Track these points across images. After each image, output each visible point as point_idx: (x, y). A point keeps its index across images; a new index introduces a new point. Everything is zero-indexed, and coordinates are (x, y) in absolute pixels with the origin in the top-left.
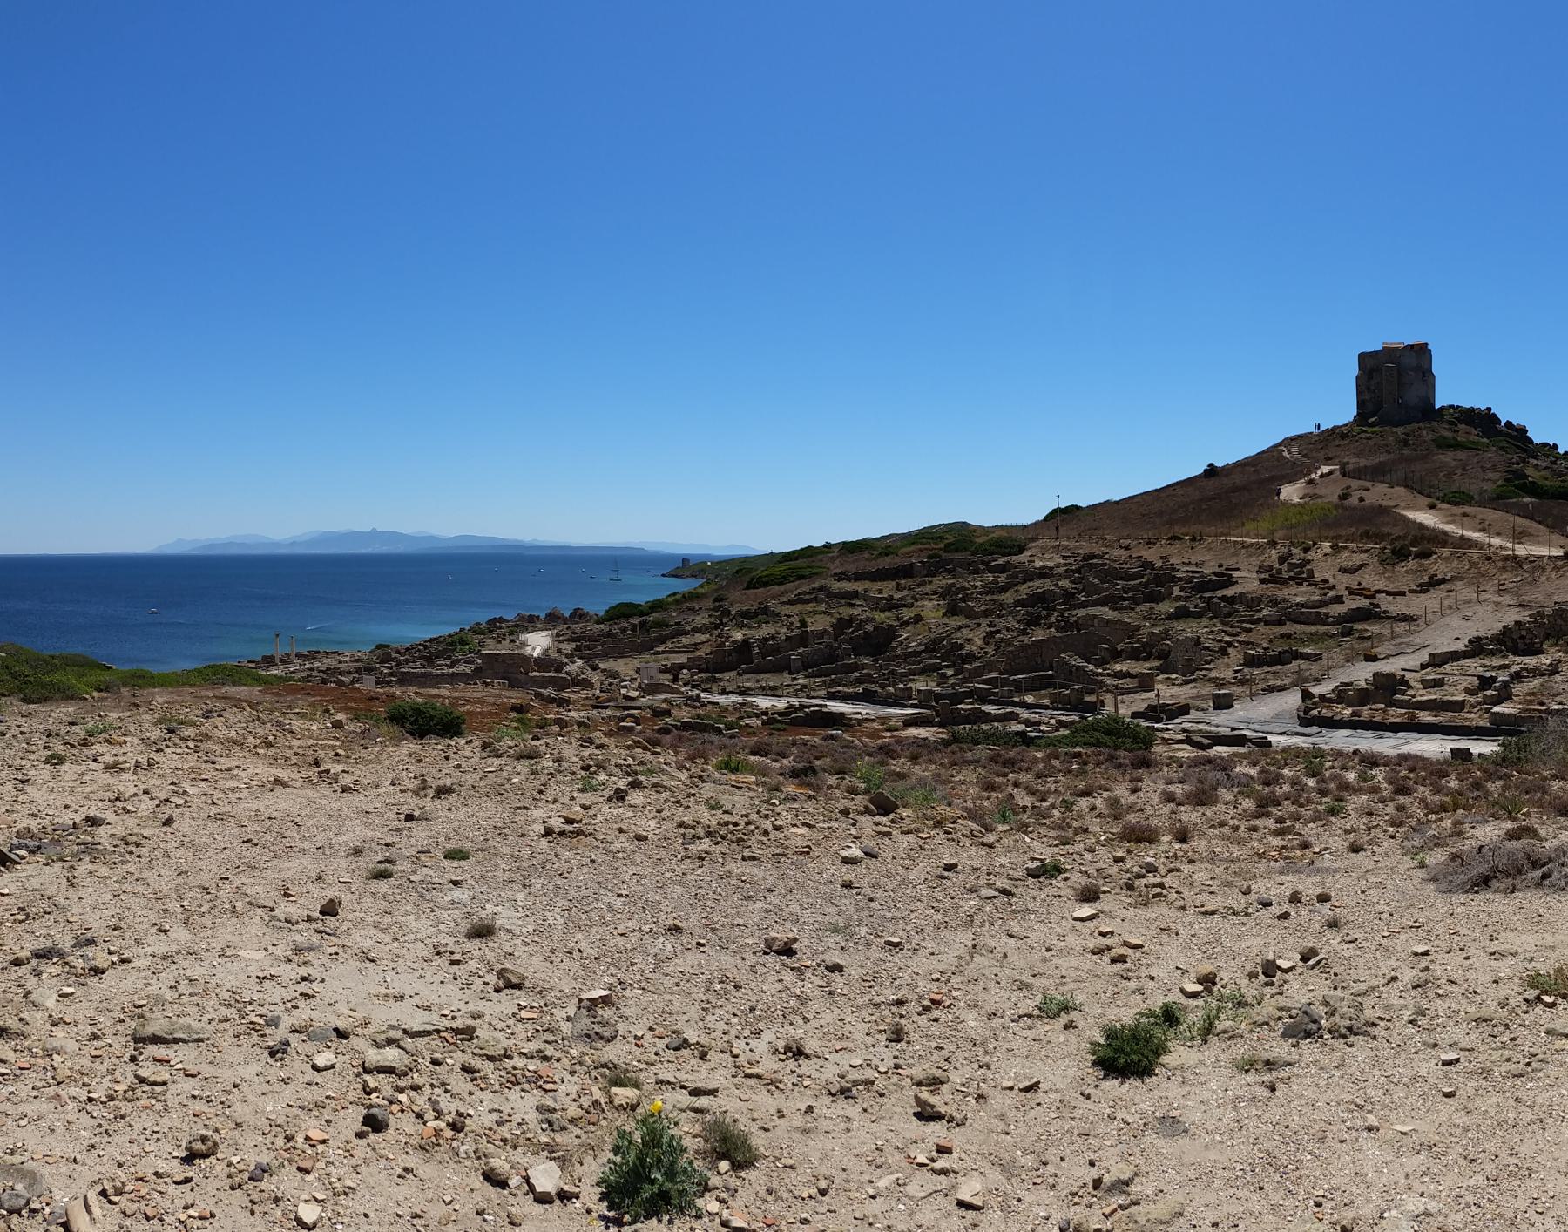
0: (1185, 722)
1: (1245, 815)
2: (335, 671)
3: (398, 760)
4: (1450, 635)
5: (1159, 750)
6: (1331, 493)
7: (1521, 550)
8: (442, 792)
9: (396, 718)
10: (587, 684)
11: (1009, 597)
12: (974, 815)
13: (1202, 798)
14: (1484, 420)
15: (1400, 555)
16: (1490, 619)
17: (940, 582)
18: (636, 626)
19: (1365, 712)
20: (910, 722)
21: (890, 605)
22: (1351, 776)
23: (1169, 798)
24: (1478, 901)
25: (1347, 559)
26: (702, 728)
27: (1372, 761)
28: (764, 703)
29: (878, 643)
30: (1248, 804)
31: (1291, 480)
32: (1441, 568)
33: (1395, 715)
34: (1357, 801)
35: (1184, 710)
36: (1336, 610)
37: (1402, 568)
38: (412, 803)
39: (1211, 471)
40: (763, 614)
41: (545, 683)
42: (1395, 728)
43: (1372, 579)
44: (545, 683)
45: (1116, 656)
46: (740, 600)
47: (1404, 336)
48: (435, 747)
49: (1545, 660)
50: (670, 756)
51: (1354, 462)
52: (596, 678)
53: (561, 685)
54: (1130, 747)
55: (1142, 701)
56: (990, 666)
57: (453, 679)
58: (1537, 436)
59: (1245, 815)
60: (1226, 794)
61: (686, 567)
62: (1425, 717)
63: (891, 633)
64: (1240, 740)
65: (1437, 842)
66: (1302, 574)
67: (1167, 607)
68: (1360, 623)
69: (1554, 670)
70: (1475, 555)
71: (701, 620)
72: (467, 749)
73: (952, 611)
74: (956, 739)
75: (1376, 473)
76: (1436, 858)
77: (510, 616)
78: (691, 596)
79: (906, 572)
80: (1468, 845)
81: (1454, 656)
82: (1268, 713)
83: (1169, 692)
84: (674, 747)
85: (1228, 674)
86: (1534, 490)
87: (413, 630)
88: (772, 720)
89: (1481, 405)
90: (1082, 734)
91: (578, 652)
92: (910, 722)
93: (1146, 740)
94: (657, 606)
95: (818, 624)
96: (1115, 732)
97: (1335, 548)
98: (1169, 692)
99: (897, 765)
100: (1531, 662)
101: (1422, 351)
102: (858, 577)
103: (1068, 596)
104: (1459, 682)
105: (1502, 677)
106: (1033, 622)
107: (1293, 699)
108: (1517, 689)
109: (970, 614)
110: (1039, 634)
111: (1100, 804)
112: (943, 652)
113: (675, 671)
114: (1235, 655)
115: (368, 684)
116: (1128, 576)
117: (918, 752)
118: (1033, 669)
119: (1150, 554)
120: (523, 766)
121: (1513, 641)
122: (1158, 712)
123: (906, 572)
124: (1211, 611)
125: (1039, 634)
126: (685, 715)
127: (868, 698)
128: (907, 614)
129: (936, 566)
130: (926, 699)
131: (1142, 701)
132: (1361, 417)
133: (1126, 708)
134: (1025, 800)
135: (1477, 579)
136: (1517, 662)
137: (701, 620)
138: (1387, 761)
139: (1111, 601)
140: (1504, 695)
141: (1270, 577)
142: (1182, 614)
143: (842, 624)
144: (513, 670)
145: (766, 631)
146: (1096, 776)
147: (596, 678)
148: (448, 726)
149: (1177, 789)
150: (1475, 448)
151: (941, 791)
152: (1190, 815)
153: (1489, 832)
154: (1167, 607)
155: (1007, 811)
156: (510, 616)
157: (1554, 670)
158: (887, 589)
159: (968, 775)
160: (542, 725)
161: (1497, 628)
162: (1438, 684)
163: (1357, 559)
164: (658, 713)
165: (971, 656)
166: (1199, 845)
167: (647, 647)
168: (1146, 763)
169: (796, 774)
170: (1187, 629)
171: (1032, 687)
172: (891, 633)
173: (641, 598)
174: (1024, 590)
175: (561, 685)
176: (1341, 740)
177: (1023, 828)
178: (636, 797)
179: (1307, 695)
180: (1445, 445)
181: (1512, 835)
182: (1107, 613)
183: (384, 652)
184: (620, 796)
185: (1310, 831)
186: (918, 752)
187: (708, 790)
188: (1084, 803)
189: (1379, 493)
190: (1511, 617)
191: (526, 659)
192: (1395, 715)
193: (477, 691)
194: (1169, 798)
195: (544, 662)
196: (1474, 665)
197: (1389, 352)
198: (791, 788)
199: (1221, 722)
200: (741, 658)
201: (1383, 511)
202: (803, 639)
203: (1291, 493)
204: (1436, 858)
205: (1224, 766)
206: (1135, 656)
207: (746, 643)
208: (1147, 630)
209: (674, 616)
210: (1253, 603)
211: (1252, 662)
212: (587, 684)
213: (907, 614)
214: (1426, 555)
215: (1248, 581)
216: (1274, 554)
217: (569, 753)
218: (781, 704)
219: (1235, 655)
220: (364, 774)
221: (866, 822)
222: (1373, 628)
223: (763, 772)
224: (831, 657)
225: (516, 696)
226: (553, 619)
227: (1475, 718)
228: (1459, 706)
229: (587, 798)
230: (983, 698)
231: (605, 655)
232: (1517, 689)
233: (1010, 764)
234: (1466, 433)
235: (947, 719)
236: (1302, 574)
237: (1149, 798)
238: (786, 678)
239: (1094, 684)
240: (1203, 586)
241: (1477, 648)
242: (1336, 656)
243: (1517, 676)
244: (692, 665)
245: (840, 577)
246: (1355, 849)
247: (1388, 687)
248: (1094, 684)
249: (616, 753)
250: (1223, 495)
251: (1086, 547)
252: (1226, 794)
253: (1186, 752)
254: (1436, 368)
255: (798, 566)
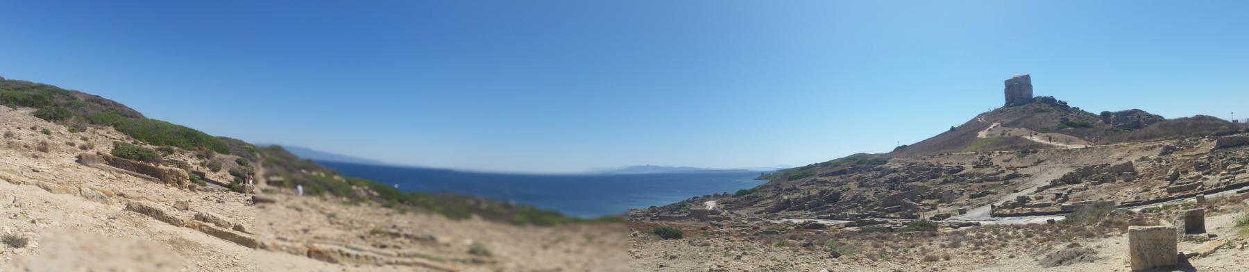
0: (949, 220)
1: (971, 249)
2: (636, 216)
3: (660, 246)
4: (1045, 180)
5: (940, 230)
6: (998, 133)
7: (1070, 147)
8: (672, 258)
9: (657, 233)
10: (729, 219)
11: (882, 180)
12: (869, 256)
13: (955, 245)
14: (1050, 101)
15: (1025, 153)
16: (1058, 173)
17: (856, 175)
18: (747, 198)
19: (1015, 211)
20: (847, 225)
21: (839, 185)
22: (1010, 233)
23: (943, 246)
24: (1059, 268)
25: (1005, 157)
26: (771, 233)
27: (1018, 227)
28: (795, 221)
29: (835, 198)
30: (972, 246)
31: (982, 129)
32: (1041, 156)
33: (1026, 210)
34: (1011, 242)
35: (949, 216)
36: (1002, 175)
37: (1027, 157)
38: (663, 261)
39: (953, 129)
40: (794, 190)
41: (713, 219)
42: (1026, 215)
43: (1015, 163)
44: (713, 219)
45: (923, 198)
46: (786, 185)
47: (1020, 73)
48: (671, 242)
49: (1083, 185)
50: (757, 243)
51: (1006, 121)
52: (732, 216)
53: (719, 220)
54: (929, 230)
55: (933, 213)
56: (877, 204)
57: (680, 218)
58: (1071, 105)
59: (971, 249)
60: (964, 243)
61: (763, 176)
62: (1037, 210)
63: (839, 195)
64: (970, 224)
65: (1042, 252)
66: (988, 164)
67: (940, 180)
68: (1011, 179)
69: (1086, 188)
70: (1053, 150)
71: (769, 195)
72: (683, 243)
73: (861, 185)
74: (863, 230)
75: (1014, 124)
76: (1042, 257)
77: (701, 196)
78: (765, 186)
79: (844, 172)
80: (1053, 252)
81: (1046, 187)
82: (980, 214)
83: (942, 210)
84: (759, 240)
85: (964, 202)
86: (1072, 125)
87: (664, 201)
88: (798, 227)
89: (1048, 95)
90: (910, 227)
91: (726, 208)
92: (847, 225)
93: (935, 227)
94: (753, 190)
95: (814, 192)
96: (924, 225)
97: (1001, 154)
98: (942, 210)
99: (841, 241)
100: (1076, 186)
101: (1027, 78)
102: (827, 175)
103: (905, 179)
104: (1048, 197)
105: (1065, 193)
106: (892, 188)
107: (988, 208)
108: (1070, 196)
109: (868, 186)
110: (894, 193)
111: (918, 250)
112: (858, 200)
113: (761, 212)
114: (966, 195)
115: (648, 220)
116: (925, 170)
117: (850, 235)
118: (892, 205)
119: (933, 161)
120: (703, 249)
121: (1068, 179)
122: (938, 217)
123: (844, 172)
124: (956, 180)
125: (894, 193)
126: (764, 228)
127: (832, 218)
128: (844, 187)
129: (854, 170)
130: (852, 217)
131: (933, 213)
132: (1007, 105)
133: (927, 216)
134: (889, 250)
135: (1055, 159)
136: (1069, 187)
137: (769, 195)
138: (1023, 227)
139: (920, 179)
140: (1066, 199)
141: (977, 166)
142: (946, 182)
143: (822, 193)
144: (702, 215)
145: (796, 195)
146: (916, 240)
147: (732, 216)
148: (677, 235)
149: (946, 243)
150: (1048, 111)
151: (858, 248)
152: (950, 251)
153: (1061, 247)
154: (940, 180)
155: (883, 254)
156: (701, 196)
157: (1086, 188)
158: (837, 179)
159: (868, 243)
160: (713, 234)
161: (1061, 175)
162: (1041, 198)
163: (1009, 156)
164: (755, 228)
165: (869, 201)
166: (953, 261)
167: (751, 205)
168: (934, 235)
169: (805, 245)
170: (948, 187)
171: (893, 211)
172: (839, 195)
173: (748, 188)
174: (888, 177)
175: (719, 220)
176: (1007, 221)
177: (888, 259)
178: (745, 258)
179: (993, 207)
180: (1038, 111)
181: (1070, 247)
182: (919, 184)
183: (653, 209)
184: (739, 258)
185: (995, 252)
186: (850, 235)
187: (771, 254)
188: (912, 250)
189: (1015, 132)
190: (1067, 171)
191: (706, 211)
192: (1026, 210)
193: (689, 223)
194: (943, 246)
195: (713, 212)
196: (1054, 190)
197: (1016, 79)
198: (802, 251)
199: (962, 219)
200: (787, 206)
201: (1017, 138)
202: (809, 198)
203: (982, 134)
204: (1042, 257)
205: (963, 234)
206: (930, 198)
207: (788, 201)
208: (933, 189)
209: (760, 194)
210: (971, 175)
211: (972, 197)
212: (729, 219)
213: (844, 187)
214: (1035, 152)
215: (969, 168)
216: (978, 157)
217: (720, 244)
218: (801, 221)
219: (966, 195)
220: (644, 252)
221: (829, 261)
222: (1016, 181)
223: (793, 245)
224: (819, 204)
225: (703, 225)
226: (716, 196)
227: (1055, 209)
228: (1049, 205)
229: (726, 259)
230: (875, 216)
231: (736, 209)
232: (1070, 196)
233: (885, 238)
234: (1045, 106)
235: (861, 224)
236: (988, 164)
237: (935, 247)
238: (803, 212)
239: (916, 209)
240: (953, 171)
241: (1054, 184)
242: (1003, 192)
243: (1070, 192)
244: (766, 211)
245: (821, 176)
246: (1012, 257)
247: (1023, 201)
248: (916, 209)
249: (738, 243)
250: (959, 137)
251: (910, 160)
252: (964, 243)
253: (950, 230)
254: (1033, 84)
255: (806, 172)
